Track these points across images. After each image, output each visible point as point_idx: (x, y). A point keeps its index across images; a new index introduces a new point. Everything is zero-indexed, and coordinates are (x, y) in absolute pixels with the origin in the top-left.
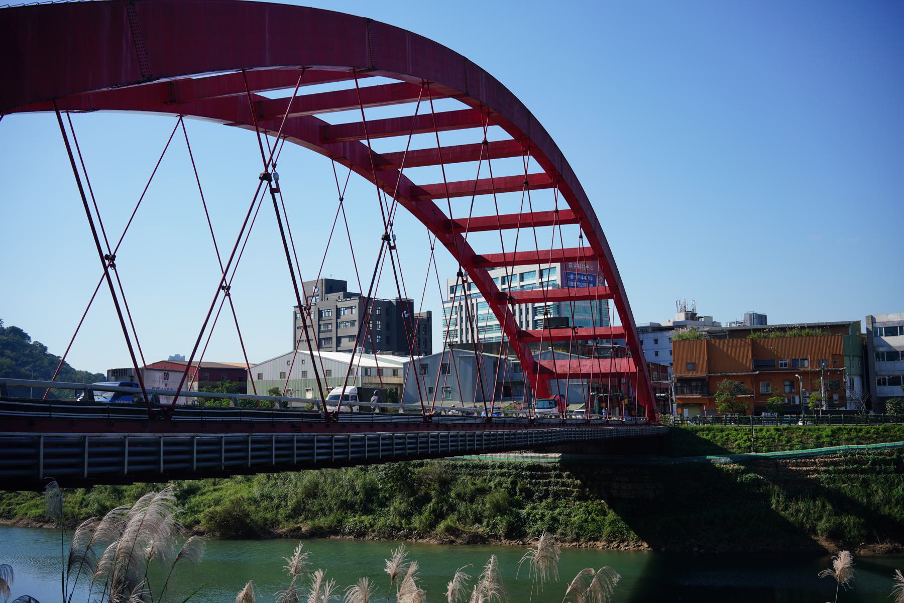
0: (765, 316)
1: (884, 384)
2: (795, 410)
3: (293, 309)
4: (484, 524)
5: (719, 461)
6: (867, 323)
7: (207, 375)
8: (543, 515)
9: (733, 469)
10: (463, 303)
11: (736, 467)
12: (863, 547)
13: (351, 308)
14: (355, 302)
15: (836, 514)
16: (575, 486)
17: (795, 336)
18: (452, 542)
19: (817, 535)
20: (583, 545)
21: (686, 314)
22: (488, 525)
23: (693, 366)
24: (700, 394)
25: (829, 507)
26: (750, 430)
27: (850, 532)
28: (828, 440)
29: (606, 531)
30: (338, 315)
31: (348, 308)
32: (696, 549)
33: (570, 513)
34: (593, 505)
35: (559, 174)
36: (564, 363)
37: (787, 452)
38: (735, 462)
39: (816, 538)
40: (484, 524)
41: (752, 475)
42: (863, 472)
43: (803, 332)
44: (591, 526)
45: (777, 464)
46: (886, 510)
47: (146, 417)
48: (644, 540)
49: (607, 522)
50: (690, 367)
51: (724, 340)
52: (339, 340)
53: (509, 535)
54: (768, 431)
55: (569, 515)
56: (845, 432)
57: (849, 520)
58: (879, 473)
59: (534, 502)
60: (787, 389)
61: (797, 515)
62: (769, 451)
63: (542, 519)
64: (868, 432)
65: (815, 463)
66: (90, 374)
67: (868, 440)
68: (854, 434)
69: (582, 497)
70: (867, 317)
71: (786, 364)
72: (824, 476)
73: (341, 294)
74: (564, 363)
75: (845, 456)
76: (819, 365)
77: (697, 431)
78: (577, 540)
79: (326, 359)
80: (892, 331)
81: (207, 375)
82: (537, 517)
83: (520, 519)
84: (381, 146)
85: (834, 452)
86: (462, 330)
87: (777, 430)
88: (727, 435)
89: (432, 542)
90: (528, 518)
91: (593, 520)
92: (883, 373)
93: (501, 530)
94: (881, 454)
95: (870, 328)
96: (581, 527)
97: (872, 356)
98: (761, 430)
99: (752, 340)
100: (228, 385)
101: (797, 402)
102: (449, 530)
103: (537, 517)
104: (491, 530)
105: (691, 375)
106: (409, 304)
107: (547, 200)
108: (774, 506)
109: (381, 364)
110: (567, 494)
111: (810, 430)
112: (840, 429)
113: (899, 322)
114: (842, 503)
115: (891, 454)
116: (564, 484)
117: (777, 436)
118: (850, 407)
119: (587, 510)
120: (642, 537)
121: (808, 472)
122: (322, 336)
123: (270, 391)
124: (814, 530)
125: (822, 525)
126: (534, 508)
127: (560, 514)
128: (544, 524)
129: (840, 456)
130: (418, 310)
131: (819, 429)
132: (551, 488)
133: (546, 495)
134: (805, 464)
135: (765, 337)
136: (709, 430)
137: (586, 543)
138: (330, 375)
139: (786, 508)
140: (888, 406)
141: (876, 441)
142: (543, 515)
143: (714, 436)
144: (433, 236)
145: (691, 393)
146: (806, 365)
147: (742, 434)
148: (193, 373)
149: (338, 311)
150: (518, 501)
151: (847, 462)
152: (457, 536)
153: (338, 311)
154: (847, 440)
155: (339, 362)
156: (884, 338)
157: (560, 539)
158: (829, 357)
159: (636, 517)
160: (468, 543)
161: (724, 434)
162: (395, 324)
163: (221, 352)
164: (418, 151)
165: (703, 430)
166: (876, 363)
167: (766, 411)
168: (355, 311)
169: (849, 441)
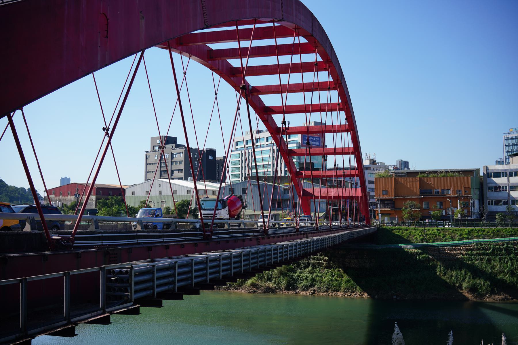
0: (408, 162)
1: (492, 204)
2: (445, 218)
3: (145, 153)
4: (273, 281)
5: (407, 247)
6: (484, 170)
7: (101, 192)
8: (307, 277)
9: (414, 252)
10: (243, 152)
11: (416, 251)
12: (488, 297)
13: (180, 153)
14: (182, 150)
15: (473, 278)
16: (325, 260)
17: (443, 176)
18: (255, 292)
19: (462, 290)
20: (331, 294)
21: (370, 161)
22: (275, 282)
23: (386, 193)
24: (390, 208)
25: (469, 274)
26: (423, 230)
27: (481, 288)
28: (466, 236)
29: (343, 286)
30: (172, 157)
31: (178, 153)
32: (395, 297)
33: (322, 276)
34: (336, 271)
35: (339, 84)
36: (318, 190)
37: (444, 243)
38: (415, 248)
39: (462, 291)
40: (273, 281)
41: (425, 255)
42: (488, 254)
43: (449, 174)
44: (335, 284)
45: (439, 250)
46: (500, 277)
47: (201, 237)
48: (365, 291)
49: (344, 282)
50: (384, 193)
51: (404, 178)
52: (172, 172)
53: (287, 288)
54: (432, 230)
55: (321, 277)
56: (475, 232)
57: (480, 281)
58: (496, 255)
59: (301, 269)
60: (439, 206)
61: (451, 279)
62: (433, 242)
63: (306, 279)
64: (488, 232)
65: (460, 249)
66: (16, 188)
67: (488, 236)
68: (480, 233)
69: (328, 267)
70: (484, 167)
71: (438, 193)
72: (465, 257)
73: (174, 145)
74: (318, 190)
75: (477, 246)
76: (457, 193)
77: (392, 230)
78: (327, 291)
79: (173, 184)
80: (497, 175)
81: (101, 192)
82: (304, 278)
83: (293, 279)
84: (235, 63)
85: (471, 243)
86: (242, 167)
87: (438, 230)
88: (410, 232)
89: (243, 291)
90: (298, 278)
91: (336, 280)
92: (491, 198)
93: (283, 285)
94: (497, 245)
95: (485, 173)
96: (329, 284)
97: (485, 188)
98: (429, 230)
99: (420, 178)
100: (115, 198)
101: (444, 214)
102: (253, 285)
103: (304, 278)
104: (278, 284)
105: (385, 197)
106: (213, 152)
107: (334, 97)
108: (438, 273)
109: (208, 188)
110: (320, 265)
111: (456, 230)
112: (473, 230)
113: (502, 170)
114: (476, 272)
115: (503, 245)
116: (318, 259)
117: (438, 234)
118: (474, 217)
119: (332, 274)
120: (364, 290)
121: (456, 254)
122: (162, 169)
123: (141, 202)
124: (460, 287)
125: (465, 285)
126: (301, 273)
127: (316, 276)
128: (308, 282)
129: (475, 246)
130: (219, 155)
131: (461, 230)
132: (310, 261)
133: (308, 265)
134: (455, 250)
135: (426, 176)
136: (400, 229)
137: (332, 293)
138: (176, 193)
139: (445, 274)
140: (497, 217)
141: (493, 237)
142: (307, 277)
143: (402, 233)
144: (258, 117)
145: (385, 207)
146: (449, 193)
147: (418, 232)
148: (94, 191)
149: (172, 155)
150: (291, 268)
151: (478, 249)
152: (258, 288)
153: (172, 155)
154: (477, 236)
155: (181, 186)
156: (493, 178)
157: (317, 291)
158: (463, 189)
159: (361, 278)
160: (264, 292)
161: (408, 232)
162: (205, 164)
163: (107, 179)
164: (259, 66)
165: (396, 229)
166: (488, 193)
167: (429, 219)
168: (183, 155)
169: (478, 237)
